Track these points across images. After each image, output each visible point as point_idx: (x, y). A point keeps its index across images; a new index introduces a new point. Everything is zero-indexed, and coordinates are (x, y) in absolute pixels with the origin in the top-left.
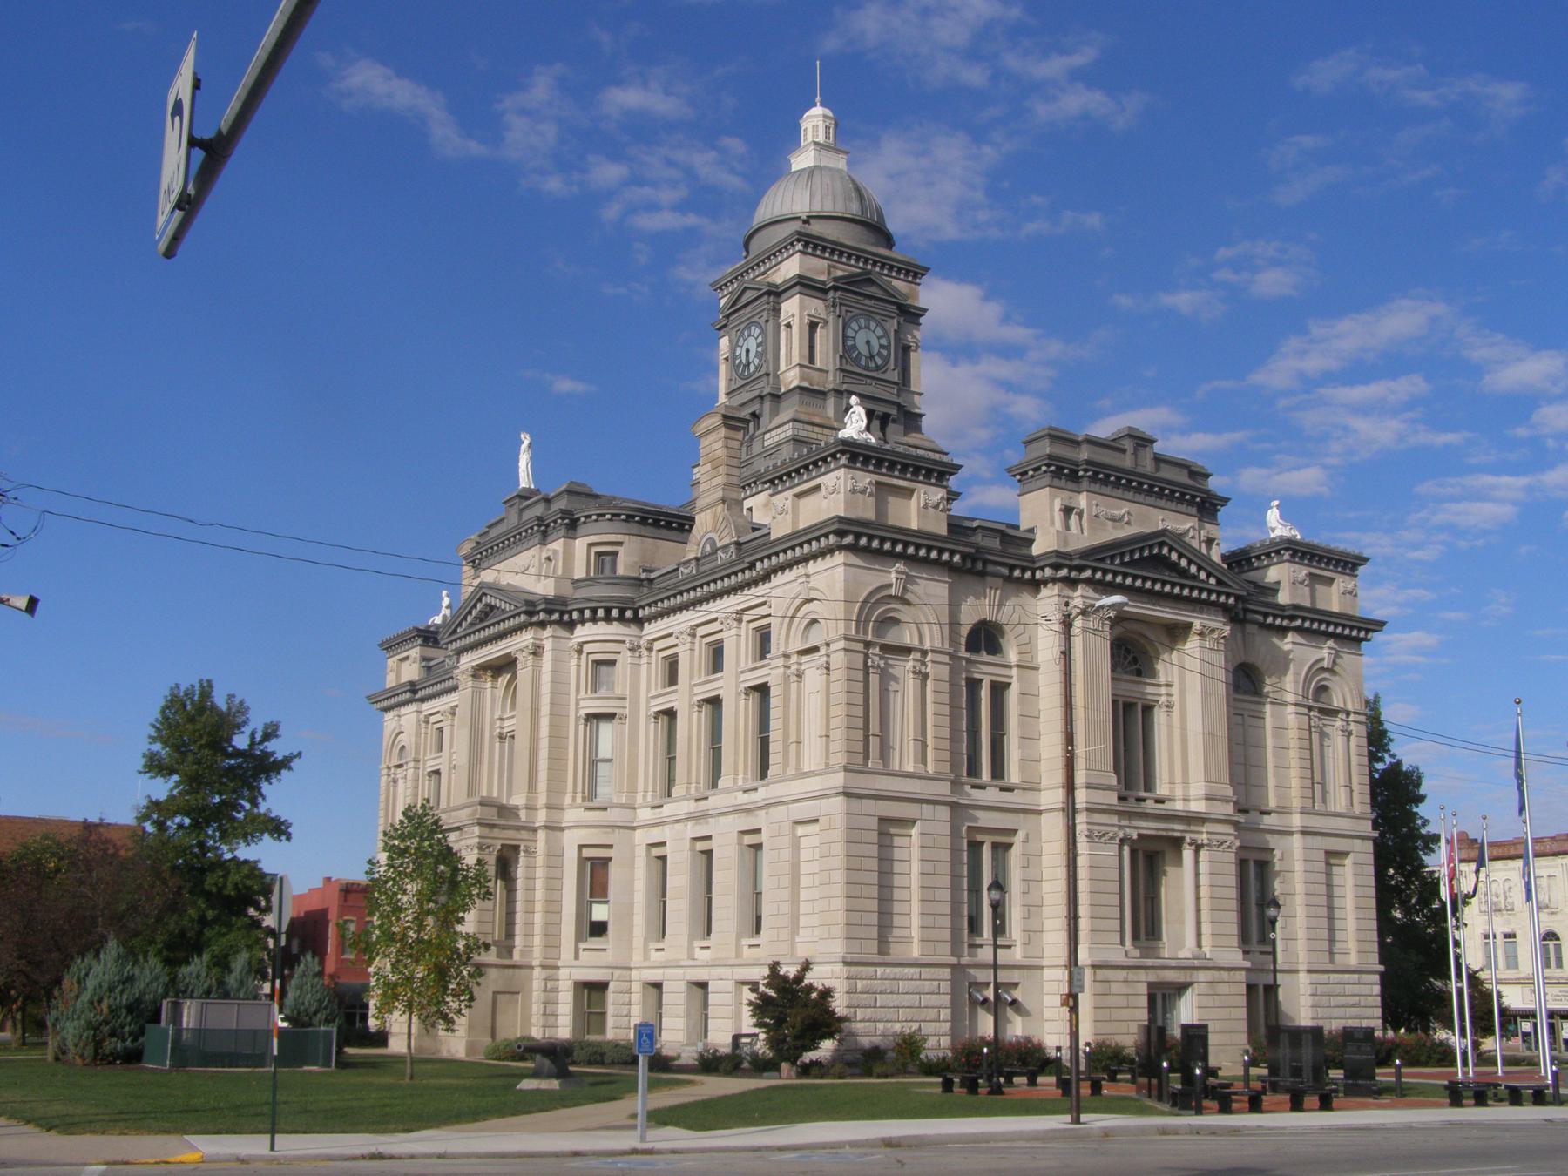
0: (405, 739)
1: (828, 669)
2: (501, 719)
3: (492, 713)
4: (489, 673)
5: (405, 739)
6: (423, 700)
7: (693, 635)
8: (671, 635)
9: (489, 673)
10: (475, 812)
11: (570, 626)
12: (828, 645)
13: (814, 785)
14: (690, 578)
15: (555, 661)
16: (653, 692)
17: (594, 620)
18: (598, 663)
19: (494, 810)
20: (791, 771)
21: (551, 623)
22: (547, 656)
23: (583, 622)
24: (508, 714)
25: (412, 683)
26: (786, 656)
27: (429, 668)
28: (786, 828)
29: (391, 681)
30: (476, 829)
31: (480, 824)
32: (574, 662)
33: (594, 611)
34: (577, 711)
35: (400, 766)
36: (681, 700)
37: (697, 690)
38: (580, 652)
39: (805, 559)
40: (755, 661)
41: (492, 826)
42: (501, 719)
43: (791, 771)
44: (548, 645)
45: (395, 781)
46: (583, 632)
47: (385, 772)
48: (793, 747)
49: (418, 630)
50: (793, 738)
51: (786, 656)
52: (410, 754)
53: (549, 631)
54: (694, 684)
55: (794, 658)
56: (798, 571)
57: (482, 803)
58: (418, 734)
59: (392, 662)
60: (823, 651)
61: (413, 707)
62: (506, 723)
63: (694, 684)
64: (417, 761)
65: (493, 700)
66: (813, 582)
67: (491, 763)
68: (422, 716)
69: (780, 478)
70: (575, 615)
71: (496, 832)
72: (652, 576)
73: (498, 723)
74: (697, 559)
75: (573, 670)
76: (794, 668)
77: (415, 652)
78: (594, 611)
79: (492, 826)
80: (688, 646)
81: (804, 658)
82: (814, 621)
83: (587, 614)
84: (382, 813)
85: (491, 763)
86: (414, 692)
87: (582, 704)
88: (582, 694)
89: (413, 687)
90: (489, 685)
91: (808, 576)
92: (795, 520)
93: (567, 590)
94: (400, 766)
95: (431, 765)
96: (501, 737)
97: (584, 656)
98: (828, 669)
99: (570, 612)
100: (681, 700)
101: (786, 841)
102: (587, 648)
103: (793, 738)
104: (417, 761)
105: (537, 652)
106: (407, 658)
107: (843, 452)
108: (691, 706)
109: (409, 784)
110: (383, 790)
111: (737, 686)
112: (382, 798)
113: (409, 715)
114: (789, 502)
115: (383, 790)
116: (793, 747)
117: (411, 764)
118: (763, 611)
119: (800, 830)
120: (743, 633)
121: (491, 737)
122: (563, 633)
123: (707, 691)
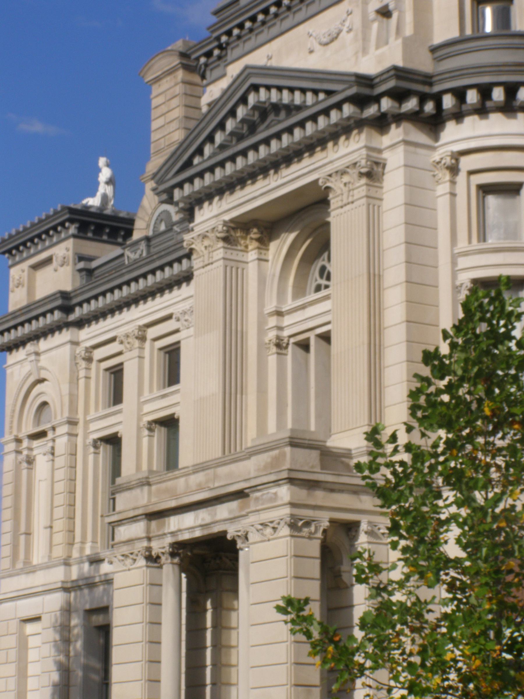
0: (48, 391)
1: (53, 454)
2: (279, 314)
3: (261, 304)
4: (254, 233)
5: (48, 391)
6: (80, 324)
7: (142, 339)
8: (169, 317)
9: (254, 233)
10: (277, 461)
11: (434, 124)
12: (54, 429)
13: (40, 579)
14: (136, 264)
15: (410, 186)
16: (93, 414)
17: (482, 111)
18: (486, 190)
19: (315, 454)
20: (20, 565)
21: (399, 118)
22: (394, 180)
23: (458, 116)
24: (290, 304)
25: (64, 295)
26: (18, 441)
27: (89, 272)
28: (14, 626)
29: (17, 299)
30: (284, 492)
31: (291, 481)
32: (443, 188)
33: (485, 92)
34: (454, 275)
35: (42, 434)
36: (128, 421)
37: (147, 408)
38: (454, 170)
39: (36, 337)
40: (104, 408)
41: (312, 485)
42: (279, 314)
43: (20, 565)
44: (395, 159)
45: (30, 461)
46: (457, 135)
47: (12, 446)
48: (22, 538)
49: (72, 211)
50: (23, 529)
51: (18, 441)
52: (59, 412)
53: (396, 133)
54: (143, 399)
55: (26, 443)
56: (30, 347)
57: (294, 443)
58: (74, 380)
59: (18, 272)
60: (50, 435)
61: (65, 335)
62: (287, 320)
63: (143, 399)
64: (72, 423)
65: (262, 281)
66: (44, 360)
67: (262, 390)
68: (80, 350)
69: (55, 228)
70: (448, 101)
71: (320, 497)
72: (94, 264)
73: (273, 321)
74: (148, 239)
75: (443, 205)
76: (25, 452)
77: (64, 249)
78: (485, 92)
79: (312, 485)
80: (136, 353)
81: (35, 443)
82: (44, 404)
83: (472, 97)
84: (7, 514)
85: (262, 390)
86: (67, 309)
87: (463, 263)
88: (462, 245)
89: (65, 302)
90: (252, 255)
91: (37, 354)
92: (31, 291)
93: (424, 64)
94: (42, 434)
95: (100, 428)
96: (280, 345)
97: (462, 178)
98: (53, 454)
99: (438, 99)
100: (128, 421)
101: (12, 641)
102: (467, 163)
103: (23, 529)
104: (72, 423)
105: (373, 173)
106: (49, 261)
107: (71, 221)
108: (139, 429)
109: (60, 461)
110: (8, 477)
111: (139, 419)
112: (8, 490)
113: (56, 352)
114: (26, 273)
115: (8, 477)
116: (22, 538)
117: (64, 429)
118: (113, 348)
119: (30, 628)
120: (93, 374)
121: (262, 347)
122: (421, 137)
123: (158, 409)
